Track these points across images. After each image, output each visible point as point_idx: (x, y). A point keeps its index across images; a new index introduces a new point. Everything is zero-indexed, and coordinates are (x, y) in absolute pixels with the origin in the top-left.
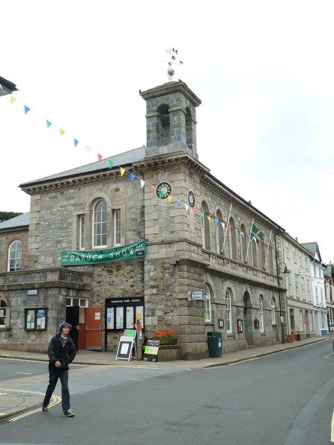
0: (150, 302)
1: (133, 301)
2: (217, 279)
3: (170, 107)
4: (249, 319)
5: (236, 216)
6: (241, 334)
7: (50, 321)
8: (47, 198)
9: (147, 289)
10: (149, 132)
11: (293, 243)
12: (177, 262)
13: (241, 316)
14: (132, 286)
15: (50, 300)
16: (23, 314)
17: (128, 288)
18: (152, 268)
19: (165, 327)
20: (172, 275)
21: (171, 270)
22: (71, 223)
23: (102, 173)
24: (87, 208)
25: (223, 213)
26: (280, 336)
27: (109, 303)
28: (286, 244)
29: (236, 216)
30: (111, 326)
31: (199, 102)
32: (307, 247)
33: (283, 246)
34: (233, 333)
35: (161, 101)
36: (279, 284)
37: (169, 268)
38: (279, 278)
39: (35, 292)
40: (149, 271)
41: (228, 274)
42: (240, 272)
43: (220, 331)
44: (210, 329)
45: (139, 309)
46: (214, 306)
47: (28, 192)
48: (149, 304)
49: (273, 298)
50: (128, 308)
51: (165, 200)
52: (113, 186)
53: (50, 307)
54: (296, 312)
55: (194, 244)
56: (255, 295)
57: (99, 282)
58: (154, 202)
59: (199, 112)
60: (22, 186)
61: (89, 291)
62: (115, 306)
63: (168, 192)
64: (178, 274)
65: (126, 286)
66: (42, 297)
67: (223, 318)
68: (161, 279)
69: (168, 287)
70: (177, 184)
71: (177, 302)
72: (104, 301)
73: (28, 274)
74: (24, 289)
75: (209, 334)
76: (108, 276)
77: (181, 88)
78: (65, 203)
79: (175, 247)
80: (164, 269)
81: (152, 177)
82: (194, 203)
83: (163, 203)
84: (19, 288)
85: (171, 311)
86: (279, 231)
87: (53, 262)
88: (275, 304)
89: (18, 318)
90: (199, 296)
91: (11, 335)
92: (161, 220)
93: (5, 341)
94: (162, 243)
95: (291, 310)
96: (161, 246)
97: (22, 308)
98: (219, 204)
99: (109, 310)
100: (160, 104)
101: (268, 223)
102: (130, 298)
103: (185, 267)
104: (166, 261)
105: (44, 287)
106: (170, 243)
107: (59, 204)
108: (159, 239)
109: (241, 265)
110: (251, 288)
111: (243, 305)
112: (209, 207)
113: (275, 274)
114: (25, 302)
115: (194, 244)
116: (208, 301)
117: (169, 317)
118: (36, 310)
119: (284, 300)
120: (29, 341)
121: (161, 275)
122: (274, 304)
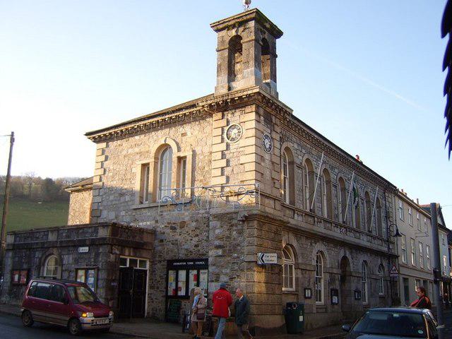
2: (303, 240)
4: (348, 289)
11: (410, 203)
13: (337, 285)
14: (196, 246)
18: (218, 224)
20: (240, 233)
25: (314, 163)
27: (172, 265)
28: (400, 203)
29: (332, 168)
31: (278, 34)
36: (389, 248)
38: (388, 242)
39: (86, 249)
40: (215, 228)
41: (316, 234)
42: (337, 233)
43: (308, 301)
44: (291, 299)
46: (299, 271)
49: (382, 264)
54: (412, 282)
56: (356, 263)
57: (162, 241)
60: (87, 134)
62: (177, 269)
67: (312, 286)
68: (228, 237)
69: (235, 247)
72: (165, 263)
75: (289, 305)
80: (232, 226)
87: (116, 218)
90: (272, 259)
98: (309, 153)
99: (170, 272)
104: (234, 216)
109: (337, 225)
110: (351, 253)
111: (339, 271)
113: (384, 236)
116: (291, 267)
118: (87, 270)
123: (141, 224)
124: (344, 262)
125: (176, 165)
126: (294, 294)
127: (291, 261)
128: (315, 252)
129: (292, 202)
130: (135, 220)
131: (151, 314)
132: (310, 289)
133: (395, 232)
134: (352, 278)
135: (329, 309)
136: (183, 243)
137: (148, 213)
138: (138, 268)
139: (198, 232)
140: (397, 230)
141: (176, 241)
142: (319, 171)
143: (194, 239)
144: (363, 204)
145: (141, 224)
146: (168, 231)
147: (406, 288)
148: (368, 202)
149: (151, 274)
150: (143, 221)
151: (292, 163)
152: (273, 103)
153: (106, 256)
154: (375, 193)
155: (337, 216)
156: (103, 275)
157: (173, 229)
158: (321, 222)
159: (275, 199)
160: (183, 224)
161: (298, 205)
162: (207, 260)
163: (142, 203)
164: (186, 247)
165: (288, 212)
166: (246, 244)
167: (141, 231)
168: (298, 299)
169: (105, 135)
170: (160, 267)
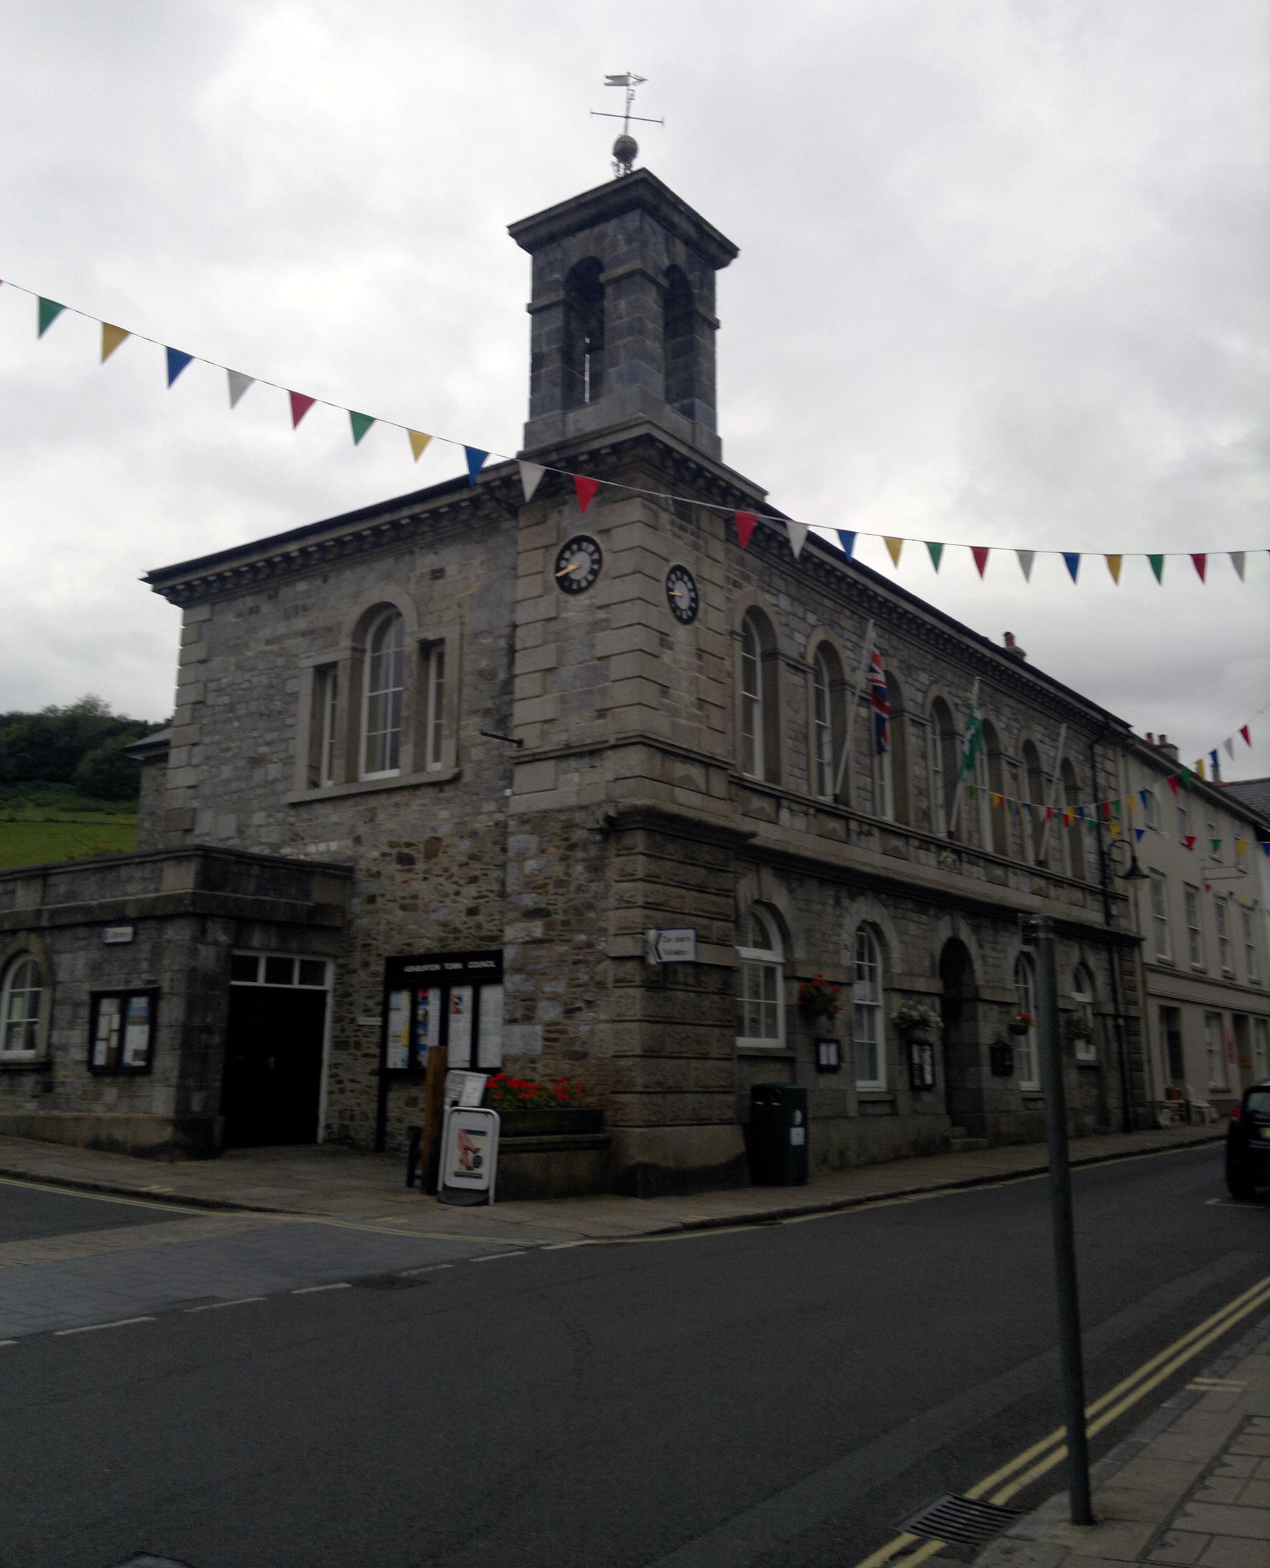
0: (518, 970)
1: (474, 965)
3: (624, 275)
5: (909, 669)
6: (927, 1097)
7: (164, 1036)
8: (228, 617)
9: (511, 922)
10: (537, 361)
12: (608, 819)
14: (472, 912)
15: (166, 962)
16: (85, 1013)
17: (460, 920)
18: (532, 842)
19: (566, 1065)
20: (596, 868)
21: (593, 852)
22: (294, 697)
23: (387, 518)
24: (346, 643)
25: (846, 655)
26: (1114, 1102)
27: (398, 974)
29: (909, 669)
30: (397, 1057)
31: (725, 252)
32: (1229, 791)
33: (1131, 779)
34: (891, 1089)
35: (576, 248)
36: (1108, 916)
37: (584, 846)
38: (1107, 897)
39: (123, 933)
40: (522, 857)
42: (926, 870)
43: (825, 1081)
45: (492, 996)
47: (174, 596)
48: (518, 978)
50: (455, 992)
51: (583, 599)
52: (427, 561)
53: (166, 989)
54: (1191, 1021)
55: (687, 757)
56: (995, 963)
57: (372, 899)
58: (545, 607)
59: (728, 284)
60: (1187, 884)
61: (338, 929)
62: (417, 987)
63: (594, 562)
64: (616, 864)
65: (453, 912)
66: (147, 947)
68: (560, 883)
70: (622, 538)
71: (608, 971)
72: (380, 968)
73: (110, 868)
74: (96, 922)
75: (760, 1092)
76: (400, 877)
77: (642, 191)
78: (281, 628)
79: (611, 765)
80: (572, 847)
81: (543, 521)
82: (694, 610)
83: (576, 608)
84: (80, 918)
85: (590, 1004)
86: (1104, 730)
88: (1094, 989)
89: (72, 1025)
91: (48, 1088)
92: (566, 673)
93: (30, 1107)
94: (567, 754)
95: (1169, 1014)
96: (564, 764)
97: (85, 989)
98: (831, 624)
100: (575, 258)
101: (1059, 702)
102: (464, 957)
103: (638, 840)
104: (579, 817)
105: (151, 917)
106: (592, 752)
107: (265, 633)
108: (557, 739)
109: (927, 843)
110: (976, 929)
112: (778, 629)
114: (95, 970)
115: (687, 757)
117: (581, 1027)
118: (124, 997)
119: (1131, 974)
120: (99, 1110)
121: (558, 870)
122: (1086, 984)
123: (312, 849)
124: (953, 960)
125: (414, 666)
126: (784, 1059)
127: (773, 956)
128: (848, 934)
129: (773, 773)
130: (295, 838)
131: (335, 1128)
132: (836, 1042)
133: (1128, 864)
134: (981, 1008)
135: (904, 1102)
136: (434, 905)
137: (332, 815)
138: (296, 985)
139: (476, 868)
140: (1134, 860)
141: (415, 897)
142: (859, 680)
143: (464, 891)
144: (1015, 777)
145: (312, 849)
146: (392, 868)
147: (1174, 1040)
148: (1035, 772)
149: (339, 1004)
150: (317, 839)
151: (771, 655)
152: (700, 471)
153: (179, 954)
154: (1056, 746)
155: (926, 815)
156: (172, 1011)
157: (406, 861)
158: (869, 834)
159: (707, 765)
160: (434, 847)
161: (792, 782)
162: (498, 956)
163: (315, 784)
164: (441, 915)
165: (757, 803)
166: (612, 902)
167: (305, 871)
168: (793, 1073)
169: (204, 580)
170: (368, 978)
